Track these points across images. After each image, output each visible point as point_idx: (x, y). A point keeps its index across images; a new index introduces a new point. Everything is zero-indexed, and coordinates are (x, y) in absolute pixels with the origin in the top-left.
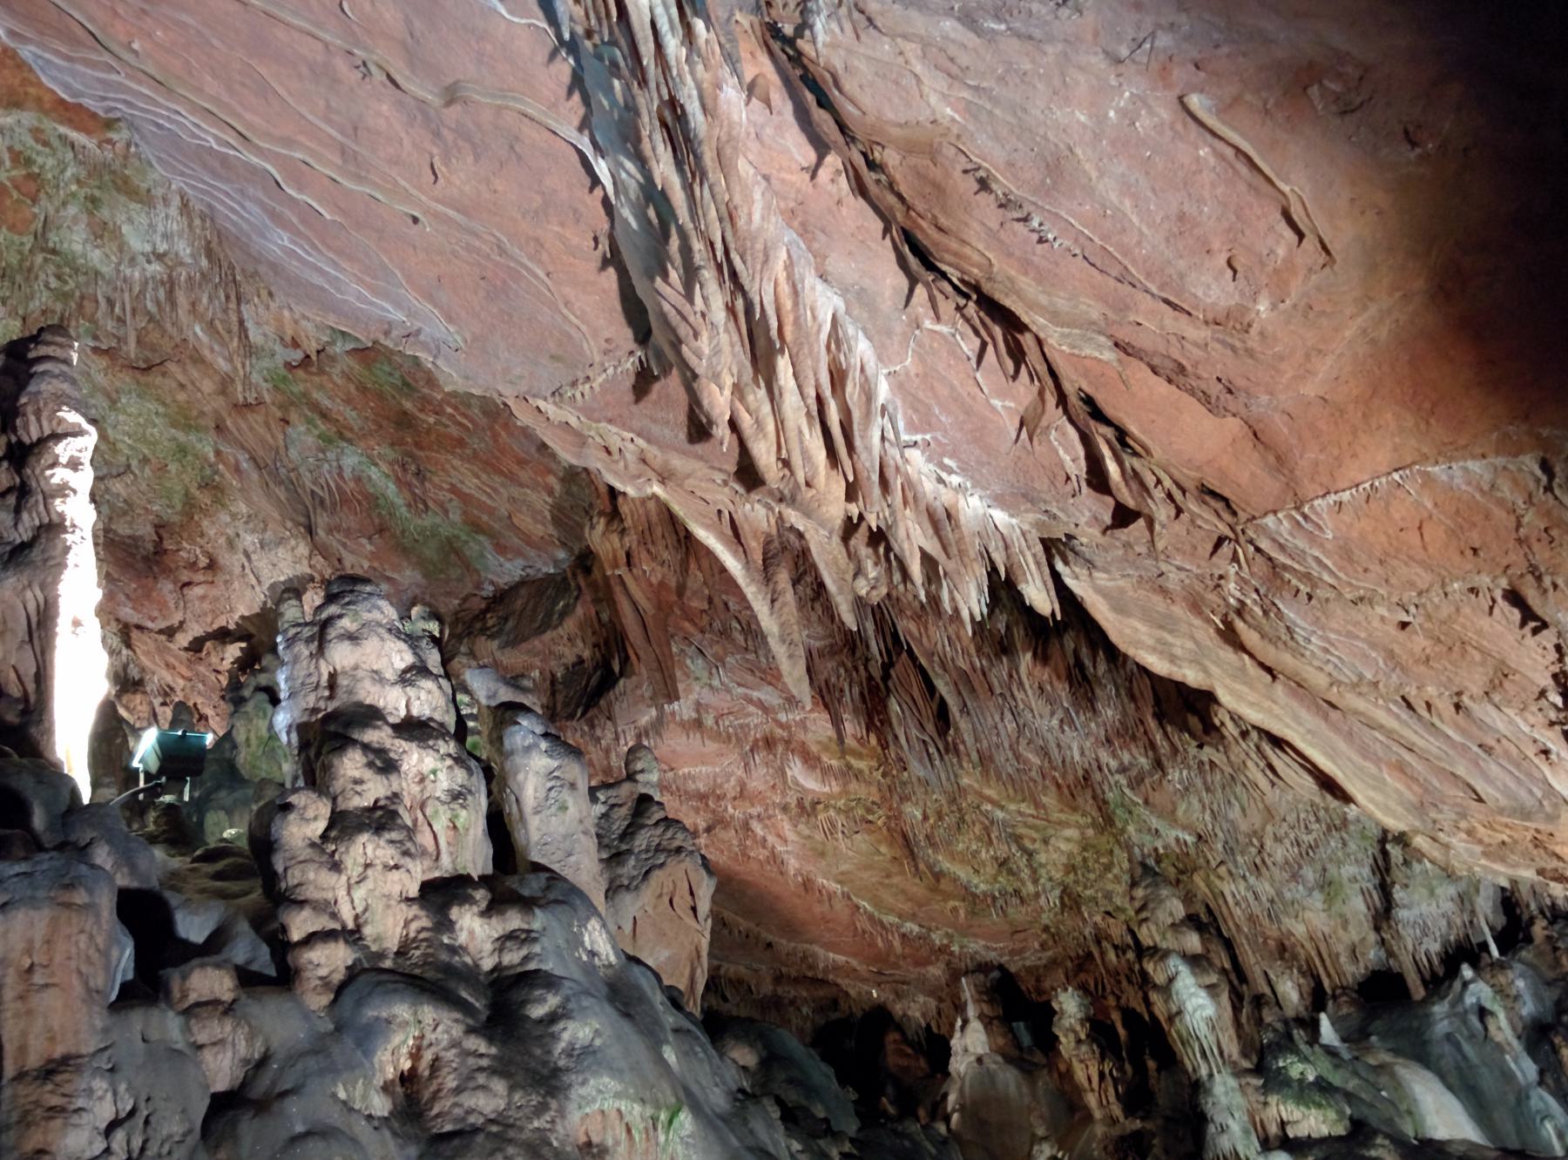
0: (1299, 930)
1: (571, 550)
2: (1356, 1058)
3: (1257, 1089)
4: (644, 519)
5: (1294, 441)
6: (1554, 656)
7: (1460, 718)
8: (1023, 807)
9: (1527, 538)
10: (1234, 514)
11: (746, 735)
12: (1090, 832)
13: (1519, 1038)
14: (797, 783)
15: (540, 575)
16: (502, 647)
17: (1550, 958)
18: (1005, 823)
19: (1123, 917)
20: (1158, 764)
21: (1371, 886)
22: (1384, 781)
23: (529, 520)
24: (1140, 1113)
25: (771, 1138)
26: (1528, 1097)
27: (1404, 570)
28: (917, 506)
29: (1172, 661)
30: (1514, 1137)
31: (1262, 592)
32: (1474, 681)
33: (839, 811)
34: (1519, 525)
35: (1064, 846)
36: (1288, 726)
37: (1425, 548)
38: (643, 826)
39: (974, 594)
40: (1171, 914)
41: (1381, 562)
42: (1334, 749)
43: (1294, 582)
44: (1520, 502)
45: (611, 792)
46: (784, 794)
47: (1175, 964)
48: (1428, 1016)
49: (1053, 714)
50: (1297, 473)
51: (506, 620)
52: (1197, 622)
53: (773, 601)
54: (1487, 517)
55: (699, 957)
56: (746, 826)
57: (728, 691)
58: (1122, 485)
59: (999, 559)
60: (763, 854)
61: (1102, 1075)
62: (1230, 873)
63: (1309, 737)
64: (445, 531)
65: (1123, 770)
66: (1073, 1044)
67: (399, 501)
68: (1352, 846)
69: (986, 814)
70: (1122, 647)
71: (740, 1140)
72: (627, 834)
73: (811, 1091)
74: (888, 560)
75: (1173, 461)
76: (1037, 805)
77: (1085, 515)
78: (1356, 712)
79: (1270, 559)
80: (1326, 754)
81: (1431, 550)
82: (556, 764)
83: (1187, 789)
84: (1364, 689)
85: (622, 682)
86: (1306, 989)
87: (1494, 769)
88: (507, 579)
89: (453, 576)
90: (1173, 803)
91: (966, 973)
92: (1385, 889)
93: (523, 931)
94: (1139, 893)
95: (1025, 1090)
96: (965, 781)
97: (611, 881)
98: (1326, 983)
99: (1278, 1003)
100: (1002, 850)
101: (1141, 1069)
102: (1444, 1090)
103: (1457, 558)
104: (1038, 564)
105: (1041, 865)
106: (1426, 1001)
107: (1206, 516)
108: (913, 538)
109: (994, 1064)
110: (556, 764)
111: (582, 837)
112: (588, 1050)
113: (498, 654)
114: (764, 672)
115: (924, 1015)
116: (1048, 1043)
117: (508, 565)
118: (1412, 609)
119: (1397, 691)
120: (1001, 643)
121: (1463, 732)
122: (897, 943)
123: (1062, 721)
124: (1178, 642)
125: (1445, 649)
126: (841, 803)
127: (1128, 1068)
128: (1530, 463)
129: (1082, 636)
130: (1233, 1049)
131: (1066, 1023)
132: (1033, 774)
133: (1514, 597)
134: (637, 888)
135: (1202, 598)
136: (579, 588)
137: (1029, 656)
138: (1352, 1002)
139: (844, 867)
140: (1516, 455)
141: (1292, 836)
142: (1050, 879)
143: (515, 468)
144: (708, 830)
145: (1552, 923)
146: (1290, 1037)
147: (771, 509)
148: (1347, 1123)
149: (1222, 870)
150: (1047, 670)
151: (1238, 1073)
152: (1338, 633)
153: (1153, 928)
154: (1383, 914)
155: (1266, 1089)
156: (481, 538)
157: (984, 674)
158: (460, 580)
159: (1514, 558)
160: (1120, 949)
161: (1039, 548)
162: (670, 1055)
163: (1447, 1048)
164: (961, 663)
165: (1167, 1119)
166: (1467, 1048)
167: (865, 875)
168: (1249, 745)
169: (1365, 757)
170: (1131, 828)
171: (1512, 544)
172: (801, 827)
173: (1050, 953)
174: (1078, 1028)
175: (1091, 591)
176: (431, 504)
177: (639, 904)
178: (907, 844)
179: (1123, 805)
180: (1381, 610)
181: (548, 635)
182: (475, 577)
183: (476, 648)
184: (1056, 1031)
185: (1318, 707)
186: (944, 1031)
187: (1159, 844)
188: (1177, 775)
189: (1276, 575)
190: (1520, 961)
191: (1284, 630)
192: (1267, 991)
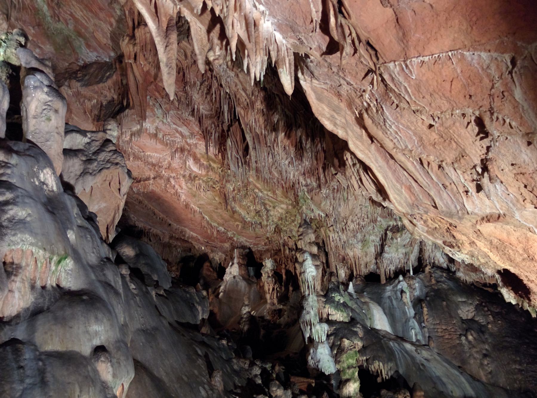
0: (351, 254)
1: (116, 53)
2: (358, 298)
3: (323, 302)
4: (144, 40)
5: (413, 26)
6: (484, 151)
7: (439, 172)
8: (269, 193)
10: (378, 59)
11: (174, 145)
12: (290, 207)
13: (411, 302)
14: (190, 168)
15: (103, 61)
16: (81, 86)
17: (428, 279)
19: (294, 239)
20: (319, 186)
21: (378, 245)
22: (402, 193)
23: (101, 35)
24: (283, 303)
25: (114, 279)
26: (409, 321)
27: (438, 100)
28: (240, 13)
30: (401, 332)
31: (379, 101)
33: (203, 181)
34: (493, 87)
35: (280, 210)
36: (372, 162)
37: (450, 92)
38: (104, 151)
39: (259, 67)
40: (310, 239)
42: (387, 176)
43: (393, 98)
44: (497, 77)
45: (93, 135)
46: (185, 171)
47: (307, 256)
48: (384, 289)
49: (287, 159)
50: (410, 43)
51: (86, 76)
52: (349, 112)
53: (166, 46)
54: (481, 82)
56: (168, 180)
57: (169, 125)
58: (335, 29)
59: (273, 55)
60: (173, 191)
61: (273, 289)
62: (334, 230)
63: (379, 168)
64: (66, 32)
65: (307, 185)
66: (266, 277)
67: (48, 14)
68: (376, 230)
69: (255, 193)
70: (316, 115)
71: (96, 276)
72: (96, 153)
73: (154, 269)
74: (226, 49)
75: (359, 25)
76: (274, 193)
77: (317, 43)
80: (384, 177)
81: (453, 92)
82: (50, 99)
83: (327, 197)
85: (127, 111)
86: (347, 274)
87: (445, 195)
88: (89, 60)
89: (67, 53)
90: (321, 201)
91: (237, 248)
92: (382, 246)
93: (4, 162)
94: (301, 230)
95: (247, 289)
96: (251, 180)
97: (84, 170)
98: (355, 273)
99: (337, 276)
100: (258, 208)
101: (287, 289)
102: (383, 314)
103: (462, 99)
104: (290, 64)
105: (271, 215)
106: (385, 285)
107: (366, 56)
108: (236, 30)
109: (239, 279)
110: (50, 99)
111: (56, 135)
112: (22, 222)
113: (80, 89)
114: (184, 120)
115: (220, 259)
116: (259, 275)
117: (90, 54)
118: (436, 119)
119: (419, 155)
120: (274, 126)
122: (215, 233)
123: (289, 162)
124: (339, 118)
125: (443, 140)
126: (205, 179)
127: (283, 288)
128: (507, 58)
129: (304, 131)
130: (318, 287)
131: (266, 270)
132: (275, 181)
133: (480, 122)
134: (95, 175)
135: (354, 101)
136: (116, 68)
137: (283, 134)
138: (362, 280)
139: (202, 202)
140: (503, 53)
141: (358, 221)
142: (273, 221)
143: (98, 11)
144: (154, 178)
145: (432, 268)
146: (338, 287)
147: (175, 4)
148: (349, 318)
149: (331, 228)
150: (289, 141)
151: (318, 296)
153: (303, 242)
154: (380, 254)
155: (326, 303)
156: (81, 39)
157: (265, 137)
158: (70, 55)
159: (485, 103)
160: (290, 250)
161: (292, 57)
162: (71, 235)
163: (388, 301)
165: (291, 306)
166: (394, 302)
167: (209, 207)
168: (354, 170)
169: (397, 181)
170: (304, 207)
172: (189, 184)
173: (267, 247)
174: (270, 272)
175: (310, 89)
176: (61, 19)
177: (95, 181)
178: (225, 198)
179: (303, 198)
181: (101, 85)
182: (76, 56)
183: (71, 84)
184: (262, 272)
185: (386, 157)
186: (225, 266)
187: (312, 215)
188: (325, 191)
189: (386, 94)
190: (419, 278)
191: (382, 121)
192: (335, 271)
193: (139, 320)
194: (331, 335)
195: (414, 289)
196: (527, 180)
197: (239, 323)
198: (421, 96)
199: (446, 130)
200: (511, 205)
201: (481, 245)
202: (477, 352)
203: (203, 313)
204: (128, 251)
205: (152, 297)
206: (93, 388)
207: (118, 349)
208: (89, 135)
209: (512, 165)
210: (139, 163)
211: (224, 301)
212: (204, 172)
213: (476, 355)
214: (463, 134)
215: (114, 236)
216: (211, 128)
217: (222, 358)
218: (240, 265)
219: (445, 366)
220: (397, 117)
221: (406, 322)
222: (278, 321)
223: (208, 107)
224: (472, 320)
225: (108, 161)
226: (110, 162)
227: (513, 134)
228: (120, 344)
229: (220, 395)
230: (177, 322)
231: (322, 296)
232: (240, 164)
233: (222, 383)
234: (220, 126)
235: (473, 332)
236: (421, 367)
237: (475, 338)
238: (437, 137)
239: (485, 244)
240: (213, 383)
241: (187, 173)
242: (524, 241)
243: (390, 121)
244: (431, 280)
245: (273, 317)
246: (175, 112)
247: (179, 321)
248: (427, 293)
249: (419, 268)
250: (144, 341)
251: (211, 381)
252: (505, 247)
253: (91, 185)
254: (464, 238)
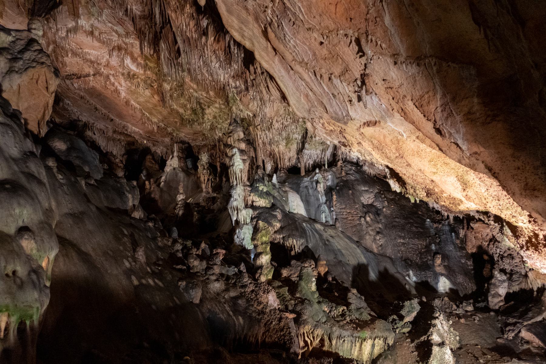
0: (276, 150)
6: (363, 67)
7: (329, 83)
8: (203, 93)
9: (369, 19)
17: (339, 171)
18: (197, 98)
20: (247, 89)
29: (242, 37)
30: (314, 215)
31: (279, 17)
32: (337, 70)
34: (368, 13)
38: (29, 50)
41: (320, 15)
43: (290, 16)
44: (371, 4)
46: (124, 69)
47: (235, 150)
52: (256, 25)
54: (359, 7)
55: (48, 106)
56: (108, 77)
60: (113, 88)
61: (208, 180)
68: (298, 128)
70: (226, 26)
71: (19, 168)
72: (22, 52)
78: (298, 73)
79: (284, 4)
81: (337, 15)
83: (254, 99)
84: (303, 65)
91: (176, 143)
94: (231, 128)
95: (186, 179)
97: (10, 68)
101: (221, 180)
103: (344, 21)
106: (304, 176)
115: (161, 153)
116: (196, 168)
118: (325, 37)
121: (329, 89)
122: (155, 128)
127: (218, 179)
130: (245, 179)
132: (207, 82)
133: (358, 42)
134: (21, 73)
142: (208, 119)
144: (94, 75)
146: (263, 179)
152: (300, 41)
154: (300, 151)
155: (251, 191)
164: (188, 34)
165: (224, 195)
166: (310, 191)
171: (363, 20)
180: (315, 35)
189: (285, 11)
191: (283, 35)
192: (262, 165)
193: (67, 206)
194: (255, 218)
195: (327, 180)
196: (394, 93)
197: (175, 209)
198: (312, 16)
199: (334, 47)
200: (383, 113)
201: (366, 145)
202: (372, 230)
203: (133, 200)
204: (60, 145)
205: (81, 186)
206: (18, 260)
207: (43, 229)
208: (13, 34)
209: (384, 80)
210: (78, 59)
211: (165, 189)
212: (142, 72)
213: (371, 233)
214: (346, 51)
215: (47, 131)
216: (145, 28)
217: (148, 237)
218: (179, 158)
219: (345, 242)
220: (295, 33)
221: (318, 207)
222: (212, 207)
223: (141, 8)
224: (371, 205)
225: (34, 61)
226: (36, 61)
227: (383, 54)
228: (45, 225)
229: (142, 265)
230: (108, 208)
231: (248, 186)
232: (173, 65)
233: (144, 257)
234: (153, 27)
235: (370, 214)
236: (327, 242)
237: (371, 219)
238: (327, 52)
239: (369, 145)
240: (136, 256)
241: (125, 72)
242: (396, 142)
243: (289, 36)
244: (341, 172)
245: (207, 204)
246: (109, 11)
247: (109, 206)
248: (338, 183)
249: (333, 163)
250: (71, 223)
251: (135, 255)
252: (383, 147)
253: (17, 84)
254: (353, 140)
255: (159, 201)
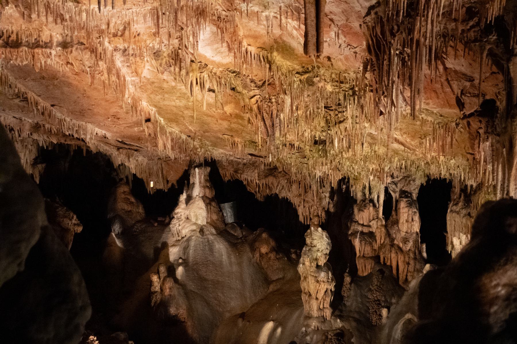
91: (199, 166)
95: (233, 260)
144: (65, 45)
218: (208, 201)
255: (189, 324)
